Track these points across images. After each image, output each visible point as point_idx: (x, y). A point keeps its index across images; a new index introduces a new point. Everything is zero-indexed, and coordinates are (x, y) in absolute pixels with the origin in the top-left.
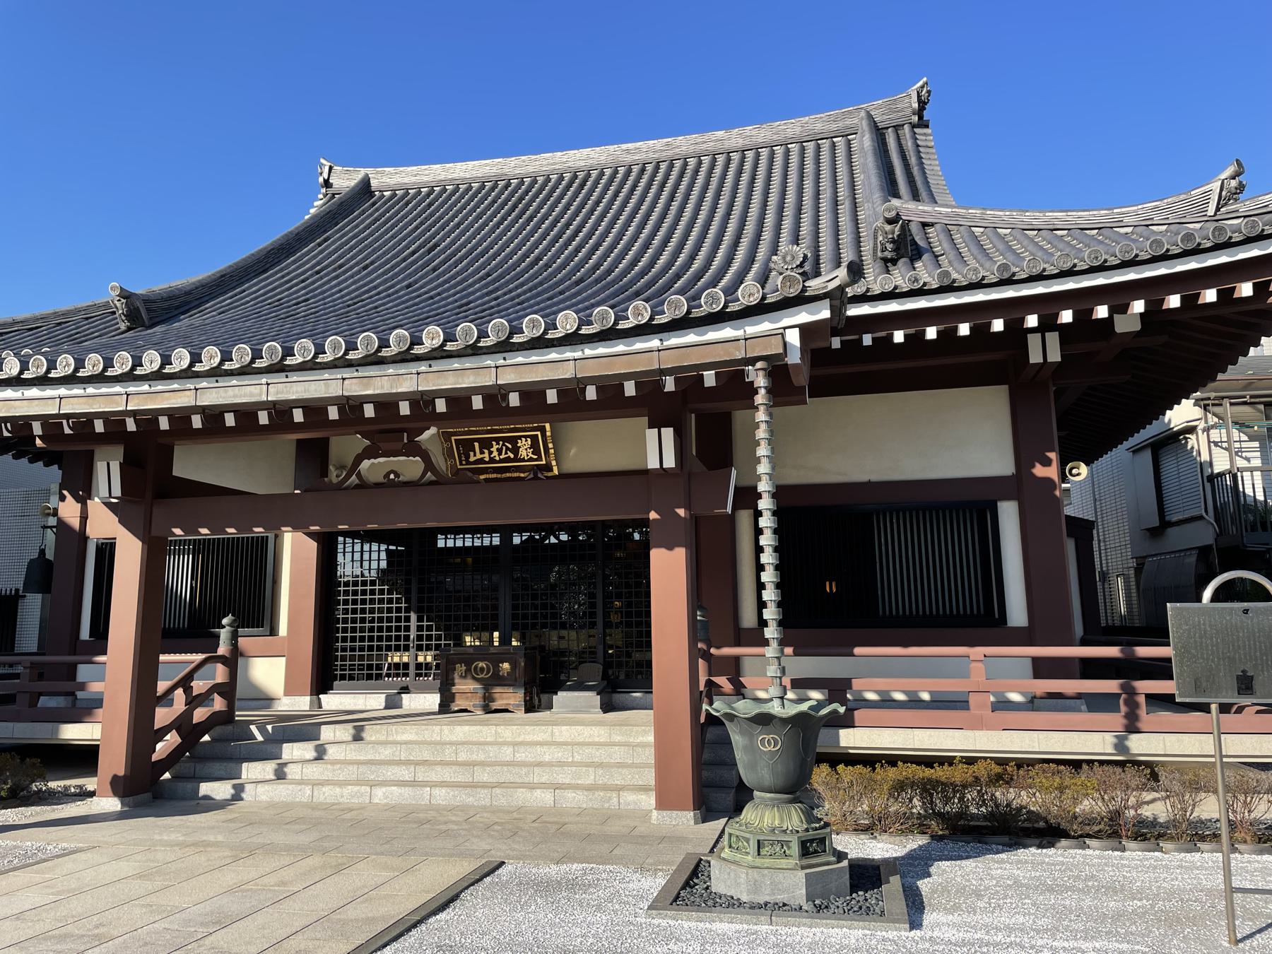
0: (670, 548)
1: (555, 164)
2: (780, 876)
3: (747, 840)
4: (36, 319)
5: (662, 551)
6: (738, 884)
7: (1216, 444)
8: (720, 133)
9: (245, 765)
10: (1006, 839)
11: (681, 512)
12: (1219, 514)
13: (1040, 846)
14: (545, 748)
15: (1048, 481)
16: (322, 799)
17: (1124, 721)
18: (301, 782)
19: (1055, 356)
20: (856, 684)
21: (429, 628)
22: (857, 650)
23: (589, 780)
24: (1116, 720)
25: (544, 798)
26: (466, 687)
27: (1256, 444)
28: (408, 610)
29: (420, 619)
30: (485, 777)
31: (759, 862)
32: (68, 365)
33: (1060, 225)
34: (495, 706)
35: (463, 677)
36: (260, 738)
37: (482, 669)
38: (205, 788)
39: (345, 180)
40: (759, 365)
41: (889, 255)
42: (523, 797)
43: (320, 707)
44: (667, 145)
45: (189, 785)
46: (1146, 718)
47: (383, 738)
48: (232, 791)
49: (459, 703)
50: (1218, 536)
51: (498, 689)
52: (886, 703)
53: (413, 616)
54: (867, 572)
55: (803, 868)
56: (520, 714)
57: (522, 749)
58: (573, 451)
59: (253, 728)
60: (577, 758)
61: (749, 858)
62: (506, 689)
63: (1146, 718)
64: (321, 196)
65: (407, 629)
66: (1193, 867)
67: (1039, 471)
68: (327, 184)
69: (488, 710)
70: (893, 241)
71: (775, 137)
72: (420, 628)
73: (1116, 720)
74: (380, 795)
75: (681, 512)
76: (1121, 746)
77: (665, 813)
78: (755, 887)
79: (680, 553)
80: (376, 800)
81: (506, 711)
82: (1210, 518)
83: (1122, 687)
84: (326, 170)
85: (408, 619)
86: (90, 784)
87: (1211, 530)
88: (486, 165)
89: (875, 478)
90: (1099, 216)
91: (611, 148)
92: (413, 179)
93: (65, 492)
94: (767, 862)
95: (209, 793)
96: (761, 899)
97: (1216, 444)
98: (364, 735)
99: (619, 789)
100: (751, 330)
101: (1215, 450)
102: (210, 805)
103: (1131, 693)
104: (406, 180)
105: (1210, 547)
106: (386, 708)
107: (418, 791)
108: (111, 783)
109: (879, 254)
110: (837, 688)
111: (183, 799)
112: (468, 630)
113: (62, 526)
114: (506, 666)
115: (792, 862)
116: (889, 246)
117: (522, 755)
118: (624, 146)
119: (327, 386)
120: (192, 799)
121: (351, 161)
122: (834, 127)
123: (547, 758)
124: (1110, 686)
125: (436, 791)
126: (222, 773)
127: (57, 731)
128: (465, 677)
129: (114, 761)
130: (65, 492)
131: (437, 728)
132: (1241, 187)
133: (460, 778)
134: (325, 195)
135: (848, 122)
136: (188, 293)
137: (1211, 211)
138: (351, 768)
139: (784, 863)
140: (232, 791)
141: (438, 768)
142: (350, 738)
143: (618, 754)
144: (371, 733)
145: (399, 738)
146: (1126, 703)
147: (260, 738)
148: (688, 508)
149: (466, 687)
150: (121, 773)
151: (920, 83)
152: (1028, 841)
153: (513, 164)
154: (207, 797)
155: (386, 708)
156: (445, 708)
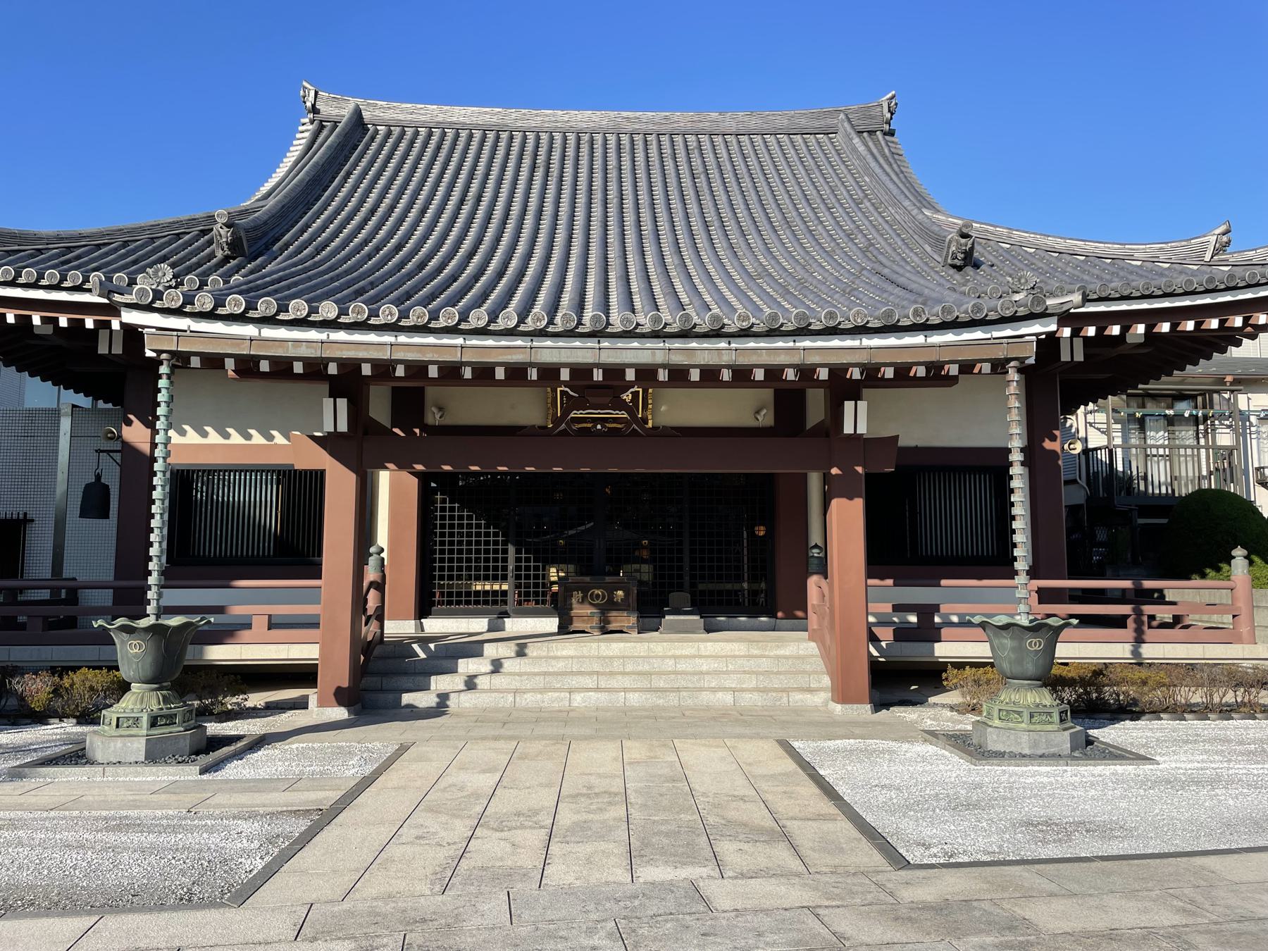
0: (851, 498)
1: (557, 122)
2: (1052, 736)
3: (1019, 713)
4: (102, 235)
5: (844, 501)
6: (1020, 744)
7: (1091, 424)
8: (714, 115)
9: (433, 678)
10: (1108, 716)
11: (860, 469)
12: (1092, 479)
13: (1132, 720)
14: (702, 661)
15: (1054, 452)
16: (524, 703)
17: (1134, 634)
18: (491, 690)
19: (1079, 357)
20: (943, 608)
21: (528, 560)
22: (943, 582)
23: (753, 684)
24: (1129, 633)
25: (728, 698)
26: (583, 612)
27: (1119, 426)
28: (505, 543)
29: (518, 551)
30: (683, 683)
31: (1032, 727)
32: (391, 314)
33: (1079, 251)
34: (612, 627)
35: (583, 601)
36: (422, 655)
37: (598, 596)
38: (407, 698)
39: (338, 109)
40: (1012, 364)
41: (958, 263)
42: (706, 698)
43: (423, 630)
44: (666, 118)
45: (391, 696)
46: (1149, 634)
47: (544, 654)
48: (437, 700)
49: (577, 625)
50: (1088, 499)
51: (614, 613)
52: (965, 624)
53: (511, 549)
54: (931, 519)
55: (1065, 729)
56: (635, 634)
57: (683, 661)
58: (663, 408)
59: (415, 646)
60: (731, 667)
61: (1023, 725)
62: (620, 613)
63: (1149, 634)
64: (307, 120)
65: (505, 560)
66: (1227, 729)
67: (1048, 444)
68: (314, 110)
69: (605, 631)
70: (965, 252)
71: (765, 126)
72: (518, 560)
73: (1129, 633)
74: (578, 699)
75: (860, 469)
76: (1136, 653)
77: (847, 706)
78: (1035, 744)
79: (858, 504)
80: (575, 704)
81: (621, 632)
82: (1083, 483)
83: (1134, 610)
84: (312, 94)
85: (505, 551)
86: (312, 695)
87: (1083, 493)
88: (486, 113)
89: (921, 444)
90: (1114, 249)
91: (612, 114)
92: (409, 117)
93: (131, 417)
94: (1038, 727)
95: (411, 702)
96: (1040, 752)
97: (1091, 424)
98: (527, 651)
99: (786, 690)
100: (996, 334)
101: (1090, 429)
102: (414, 713)
103: (1139, 613)
104: (401, 117)
105: (1081, 506)
106: (489, 631)
107: (614, 696)
108: (335, 694)
109: (949, 261)
110: (926, 612)
111: (386, 708)
112: (553, 562)
113: (128, 449)
114: (620, 593)
115: (1055, 727)
116: (960, 256)
117: (682, 666)
118: (625, 114)
119: (720, 355)
120: (394, 708)
121: (345, 90)
122: (817, 124)
123: (705, 668)
124: (1125, 609)
125: (630, 696)
126: (410, 685)
127: (201, 652)
128: (582, 602)
129: (337, 673)
130: (131, 417)
131: (594, 645)
132: (1228, 243)
133: (639, 685)
134: (312, 122)
135: (829, 121)
136: (265, 223)
137: (1207, 258)
138: (537, 678)
139: (1049, 727)
140: (437, 700)
141: (620, 677)
142: (513, 654)
143: (765, 664)
144: (533, 650)
145: (559, 654)
146: (1135, 621)
147: (422, 655)
148: (864, 467)
149: (583, 612)
150: (345, 684)
151: (889, 95)
152: (1123, 716)
153: (513, 116)
154: (409, 706)
155: (489, 631)
156: (564, 629)
